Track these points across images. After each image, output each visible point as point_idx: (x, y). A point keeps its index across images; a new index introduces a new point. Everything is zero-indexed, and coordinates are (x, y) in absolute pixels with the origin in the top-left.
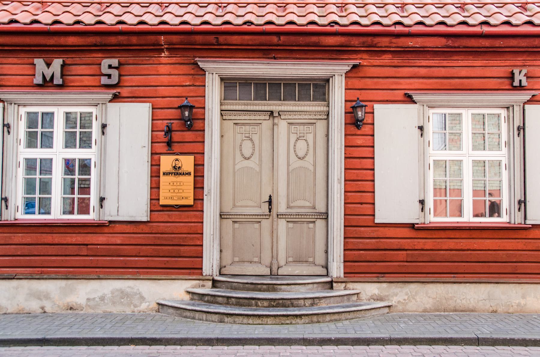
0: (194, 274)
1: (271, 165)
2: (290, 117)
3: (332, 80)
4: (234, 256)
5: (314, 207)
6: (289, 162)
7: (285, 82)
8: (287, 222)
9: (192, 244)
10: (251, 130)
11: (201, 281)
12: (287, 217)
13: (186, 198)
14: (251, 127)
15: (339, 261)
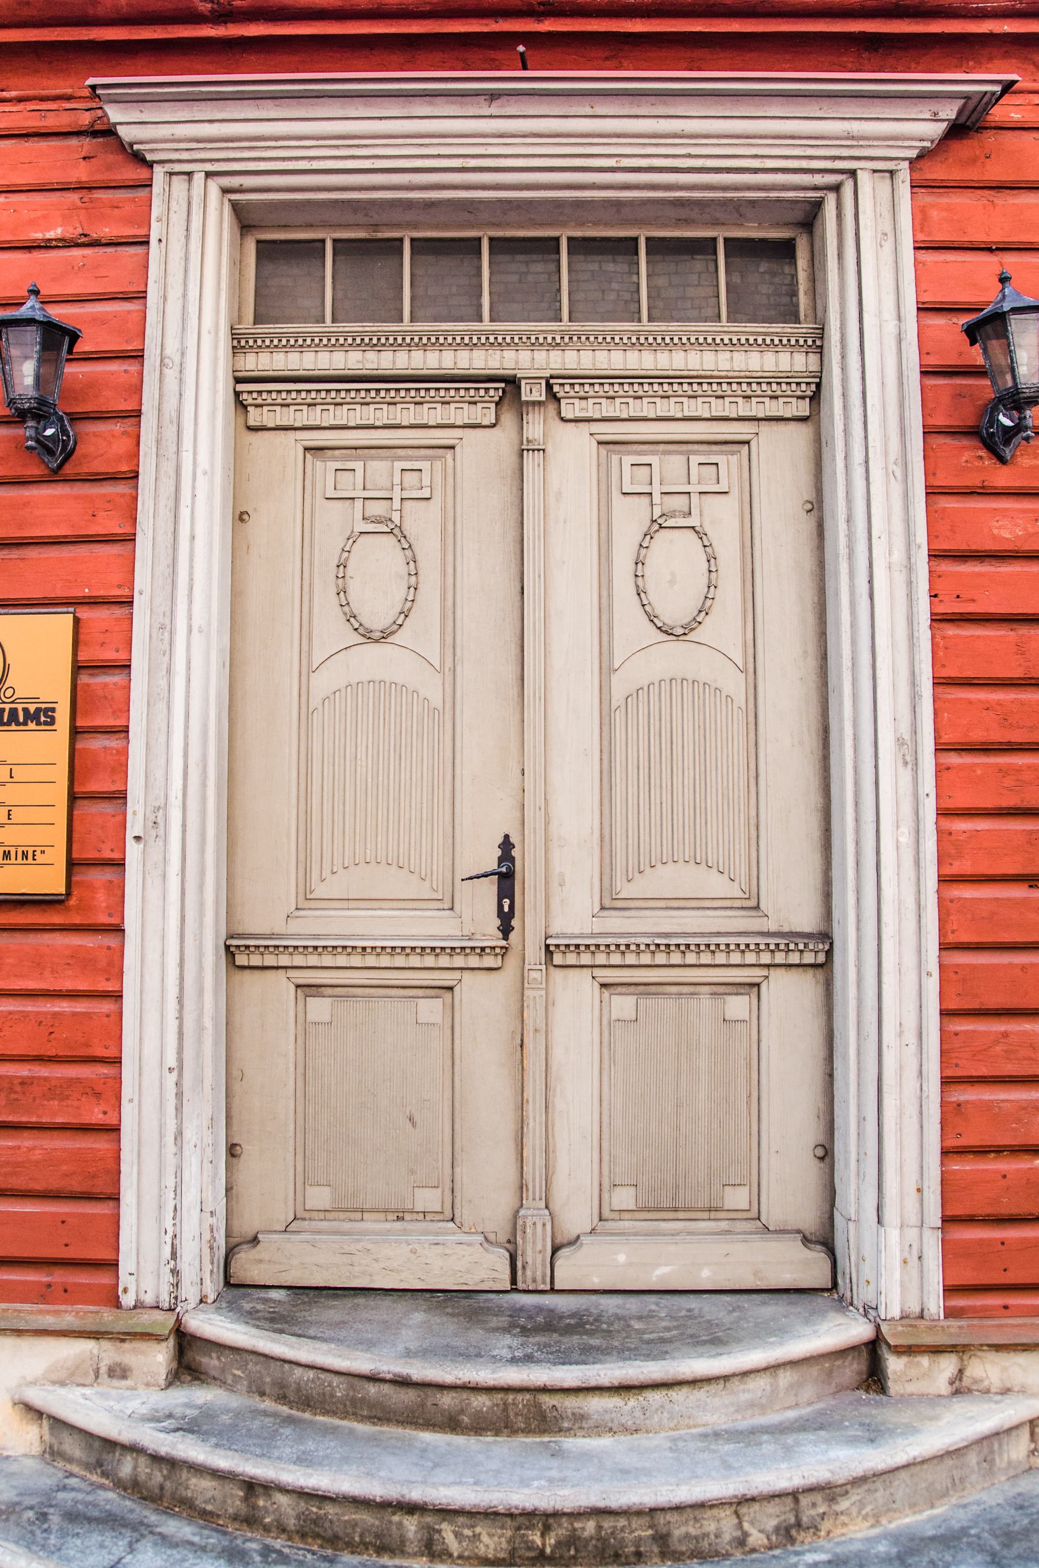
0: (68, 1295)
1: (510, 671)
2: (608, 409)
3: (839, 216)
4: (305, 1180)
5: (753, 903)
6: (611, 653)
7: (578, 233)
8: (603, 985)
9: (60, 1120)
10: (397, 480)
11: (105, 1344)
12: (601, 959)
13: (25, 855)
14: (399, 465)
15: (913, 1219)
